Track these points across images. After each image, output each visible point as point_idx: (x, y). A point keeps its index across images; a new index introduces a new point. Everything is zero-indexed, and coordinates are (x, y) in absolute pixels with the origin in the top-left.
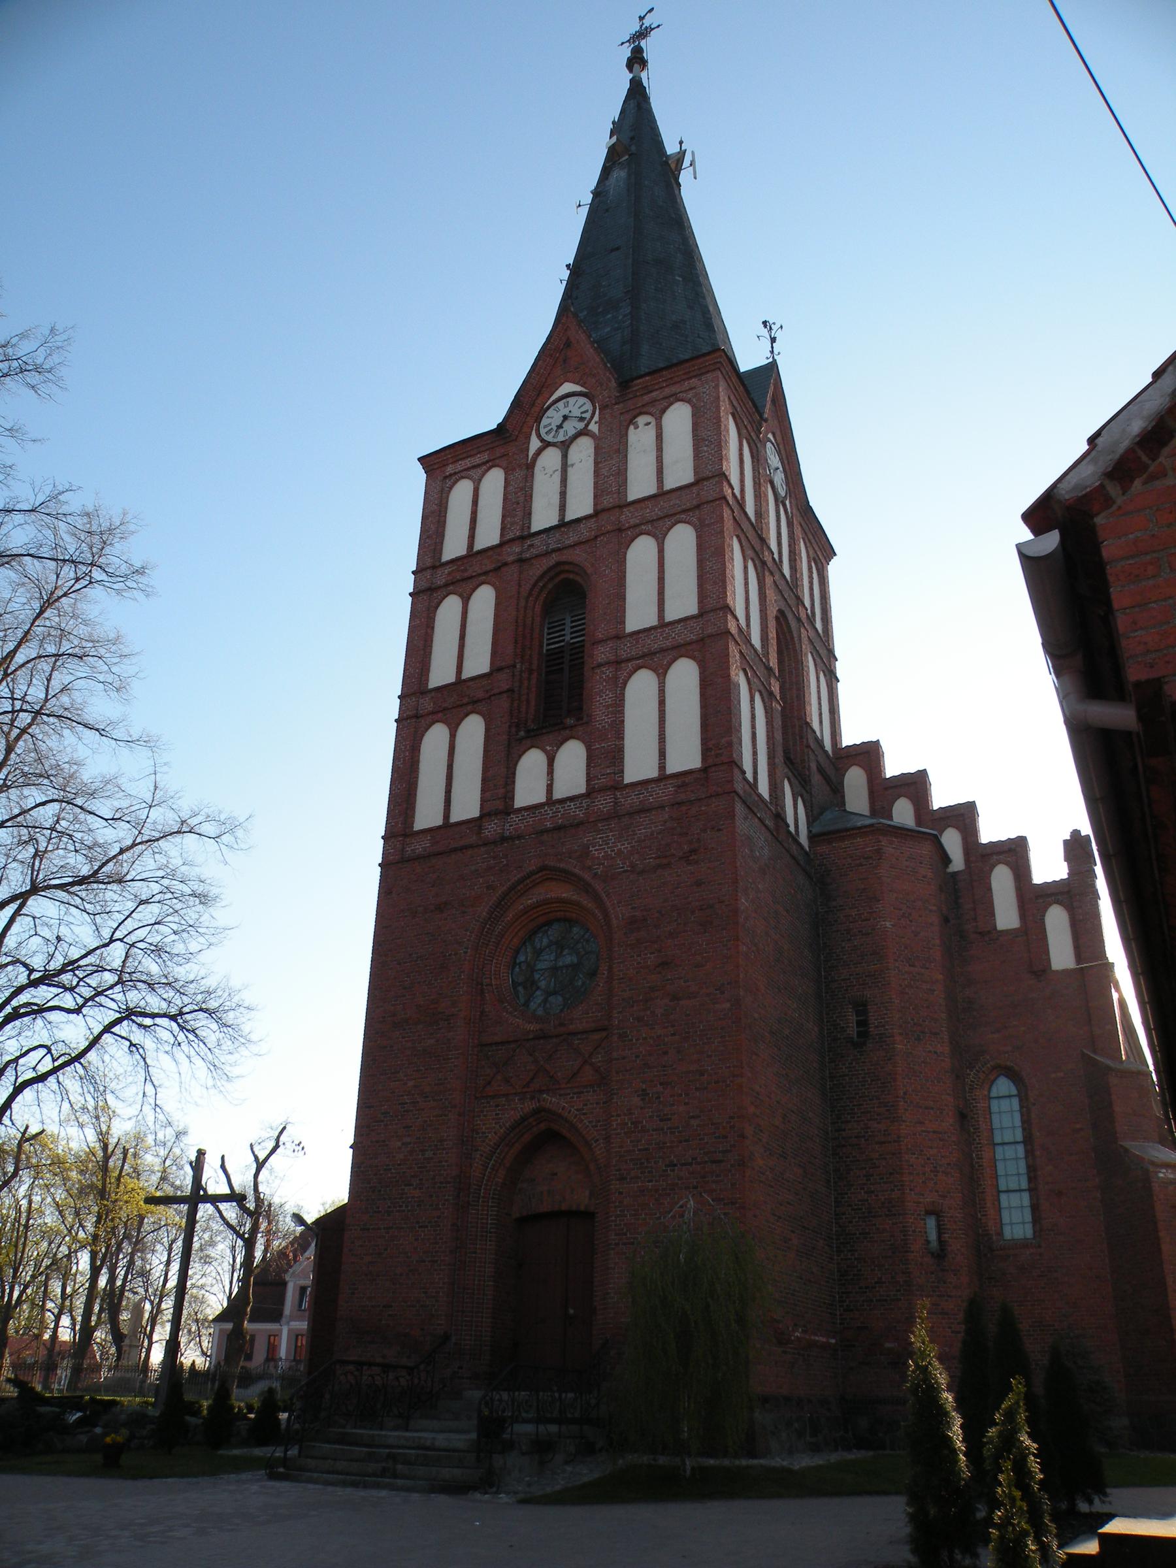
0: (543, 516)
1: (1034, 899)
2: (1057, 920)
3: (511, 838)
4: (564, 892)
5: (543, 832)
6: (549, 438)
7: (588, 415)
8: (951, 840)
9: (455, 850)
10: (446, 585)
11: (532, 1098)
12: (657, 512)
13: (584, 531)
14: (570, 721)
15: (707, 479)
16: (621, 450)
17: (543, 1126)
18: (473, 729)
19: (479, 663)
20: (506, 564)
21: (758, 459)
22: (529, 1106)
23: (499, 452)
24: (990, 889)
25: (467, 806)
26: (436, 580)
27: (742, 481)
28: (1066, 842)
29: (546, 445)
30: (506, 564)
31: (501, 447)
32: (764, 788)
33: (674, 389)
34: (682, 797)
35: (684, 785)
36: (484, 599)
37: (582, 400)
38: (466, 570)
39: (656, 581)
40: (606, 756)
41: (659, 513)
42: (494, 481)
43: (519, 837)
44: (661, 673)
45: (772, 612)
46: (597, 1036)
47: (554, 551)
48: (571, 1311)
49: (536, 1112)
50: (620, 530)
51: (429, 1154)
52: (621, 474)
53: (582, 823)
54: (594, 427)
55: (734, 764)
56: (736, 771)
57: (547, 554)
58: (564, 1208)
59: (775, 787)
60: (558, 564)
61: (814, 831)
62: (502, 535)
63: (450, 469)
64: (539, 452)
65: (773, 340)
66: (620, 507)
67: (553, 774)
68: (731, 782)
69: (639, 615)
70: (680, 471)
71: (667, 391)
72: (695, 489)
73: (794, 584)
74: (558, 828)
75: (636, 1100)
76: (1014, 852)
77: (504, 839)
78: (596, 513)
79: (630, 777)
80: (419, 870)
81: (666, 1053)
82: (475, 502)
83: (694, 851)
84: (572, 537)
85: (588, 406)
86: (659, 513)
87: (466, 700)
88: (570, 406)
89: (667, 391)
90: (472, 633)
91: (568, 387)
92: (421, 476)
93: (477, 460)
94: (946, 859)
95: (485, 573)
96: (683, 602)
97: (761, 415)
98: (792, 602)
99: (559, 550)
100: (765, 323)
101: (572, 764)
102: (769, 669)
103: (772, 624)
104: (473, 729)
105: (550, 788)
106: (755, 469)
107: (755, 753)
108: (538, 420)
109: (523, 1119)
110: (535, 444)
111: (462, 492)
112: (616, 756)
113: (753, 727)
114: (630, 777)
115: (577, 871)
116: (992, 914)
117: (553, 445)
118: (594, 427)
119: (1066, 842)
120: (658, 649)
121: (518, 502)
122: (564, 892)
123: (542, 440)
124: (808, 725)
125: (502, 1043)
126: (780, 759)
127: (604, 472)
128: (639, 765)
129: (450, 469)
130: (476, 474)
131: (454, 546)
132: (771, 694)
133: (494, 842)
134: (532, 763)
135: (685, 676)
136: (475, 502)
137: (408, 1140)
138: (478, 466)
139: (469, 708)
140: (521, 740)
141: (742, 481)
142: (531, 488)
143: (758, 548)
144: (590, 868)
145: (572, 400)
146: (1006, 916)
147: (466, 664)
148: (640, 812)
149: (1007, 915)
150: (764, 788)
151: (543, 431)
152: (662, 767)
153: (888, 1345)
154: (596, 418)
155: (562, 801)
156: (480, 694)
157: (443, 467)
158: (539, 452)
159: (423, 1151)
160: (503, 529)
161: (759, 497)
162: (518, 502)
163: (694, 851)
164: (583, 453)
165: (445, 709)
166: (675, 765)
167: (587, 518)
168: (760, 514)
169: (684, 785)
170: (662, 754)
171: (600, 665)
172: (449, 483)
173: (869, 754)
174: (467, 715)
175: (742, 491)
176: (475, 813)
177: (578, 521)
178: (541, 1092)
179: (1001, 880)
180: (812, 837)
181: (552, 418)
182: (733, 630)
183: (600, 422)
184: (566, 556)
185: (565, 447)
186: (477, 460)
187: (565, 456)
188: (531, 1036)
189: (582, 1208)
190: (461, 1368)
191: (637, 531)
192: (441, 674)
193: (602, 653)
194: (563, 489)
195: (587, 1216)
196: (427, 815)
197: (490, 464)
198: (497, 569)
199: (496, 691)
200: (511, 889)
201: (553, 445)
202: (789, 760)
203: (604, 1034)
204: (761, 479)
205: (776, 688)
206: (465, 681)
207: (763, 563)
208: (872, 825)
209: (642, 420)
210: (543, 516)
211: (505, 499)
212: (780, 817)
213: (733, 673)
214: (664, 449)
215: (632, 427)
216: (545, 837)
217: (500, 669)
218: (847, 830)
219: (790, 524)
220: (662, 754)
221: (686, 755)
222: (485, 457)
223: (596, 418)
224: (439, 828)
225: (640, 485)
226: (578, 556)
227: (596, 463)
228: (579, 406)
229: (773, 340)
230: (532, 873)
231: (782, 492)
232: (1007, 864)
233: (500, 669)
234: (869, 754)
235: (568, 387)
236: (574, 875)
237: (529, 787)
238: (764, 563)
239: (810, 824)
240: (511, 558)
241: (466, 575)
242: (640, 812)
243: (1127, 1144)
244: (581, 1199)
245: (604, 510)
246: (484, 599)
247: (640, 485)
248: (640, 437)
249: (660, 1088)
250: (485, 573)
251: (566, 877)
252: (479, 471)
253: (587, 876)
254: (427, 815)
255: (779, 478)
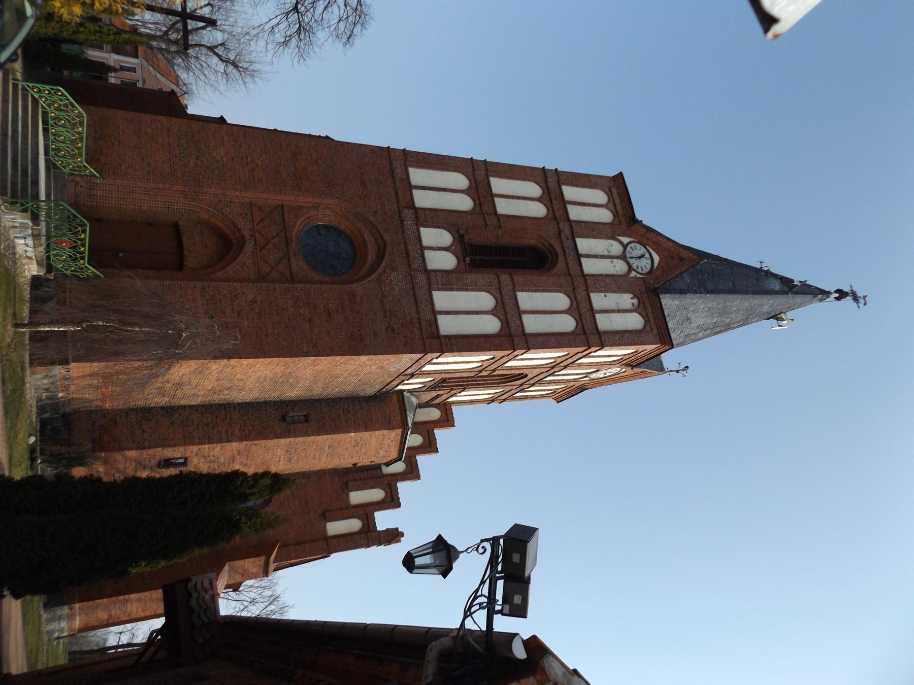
0: (584, 245)
1: (366, 512)
2: (354, 524)
3: (402, 226)
4: (371, 256)
5: (405, 244)
6: (628, 249)
7: (640, 270)
8: (399, 467)
9: (396, 193)
10: (548, 188)
11: (251, 236)
12: (583, 310)
13: (574, 270)
14: (468, 259)
15: (600, 339)
16: (619, 290)
17: (234, 241)
18: (464, 203)
19: (503, 207)
20: (558, 224)
21: (611, 364)
22: (247, 236)
23: (623, 219)
24: (371, 488)
25: (422, 199)
26: (551, 183)
27: (599, 356)
28: (397, 529)
29: (625, 247)
30: (558, 224)
31: (625, 220)
32: (428, 368)
33: (652, 319)
34: (423, 324)
35: (431, 325)
36: (538, 210)
37: (649, 267)
38: (556, 200)
39: (544, 309)
40: (448, 281)
41: (582, 311)
42: (605, 216)
43: (403, 230)
44: (493, 312)
45: (525, 372)
46: (288, 273)
47: (564, 252)
48: (121, 255)
49: (243, 238)
50: (574, 289)
51: (216, 172)
52: (606, 289)
53: (410, 266)
54: (633, 274)
55: (442, 351)
56: (438, 354)
57: (563, 247)
58: (186, 252)
59: (429, 373)
60: (557, 254)
61: (405, 393)
62: (575, 221)
63: (614, 191)
64: (621, 242)
65: (677, 371)
66: (587, 290)
67: (438, 249)
68: (432, 352)
69: (526, 299)
70: (604, 322)
71: (651, 316)
72: (595, 331)
73: (540, 382)
74: (408, 254)
75: (250, 297)
76: (392, 501)
77: (402, 221)
78: (584, 276)
79: (435, 294)
80: (385, 170)
81: (278, 314)
82: (595, 205)
83: (393, 331)
84: (572, 261)
85: (645, 271)
86: (582, 311)
87: (482, 200)
88: (645, 261)
89: (651, 316)
90: (519, 201)
91: (657, 259)
92: (612, 173)
93: (619, 207)
94: (388, 464)
95: (554, 212)
96: (532, 324)
97: (636, 366)
98: (532, 382)
99: (565, 254)
100: (687, 367)
101: (443, 261)
102: (494, 370)
103: (517, 372)
104: (464, 203)
105: (431, 248)
106: (605, 363)
107: (448, 363)
108: (639, 242)
109: (239, 230)
110: (625, 240)
111: (600, 197)
112: (448, 286)
113: (462, 362)
114: (435, 294)
115: (383, 264)
116: (357, 490)
117: (624, 251)
118: (633, 274)
119: (397, 529)
120: (506, 310)
121: (593, 230)
122: (371, 256)
123: (627, 244)
124: (464, 390)
125: (284, 219)
126: (445, 376)
127: (608, 280)
128: (442, 299)
129: (614, 191)
130: (611, 205)
131: (570, 192)
132: (481, 371)
133: (400, 216)
134: (444, 237)
135: (491, 325)
136: (595, 205)
137: (225, 159)
138: (615, 208)
139: (478, 202)
140: (458, 231)
141: (599, 356)
142: (601, 238)
143: (562, 365)
144: (384, 271)
145: (649, 261)
146: (357, 497)
147: (503, 200)
148: (416, 300)
149: (357, 497)
150: (428, 368)
151: (632, 245)
152: (441, 313)
153: (105, 437)
154: (638, 275)
155: (423, 256)
156: (485, 208)
157: (617, 188)
158: (621, 242)
159: (218, 168)
160: (579, 222)
161: (590, 365)
162: (593, 230)
163: (393, 331)
164: (619, 267)
165: (477, 187)
166: (441, 319)
167: (582, 270)
168: (580, 365)
169: (431, 325)
170: (448, 313)
171: (498, 278)
172: (607, 190)
173: (447, 420)
174: (474, 200)
175: (593, 357)
176: (418, 204)
177: (580, 265)
178: (255, 241)
179: (377, 494)
180: (402, 391)
181: (639, 250)
182: (516, 353)
183: (635, 277)
184: (561, 258)
185: (623, 257)
186: (619, 207)
187: (617, 257)
188: (288, 235)
189: (185, 263)
190: (82, 187)
191: (573, 298)
192: (498, 185)
193: (505, 278)
194: (599, 256)
195: (180, 267)
196: (417, 176)
197: (615, 214)
198: (555, 218)
199: (487, 218)
200: (374, 226)
201: (624, 251)
202: (444, 380)
203: (289, 278)
204: (599, 366)
205: (484, 373)
206: (493, 199)
207: (552, 368)
208: (407, 425)
209: (635, 301)
210: (584, 245)
211: (595, 223)
212: (412, 376)
213: (492, 352)
214: (617, 311)
215: (631, 296)
216: (403, 245)
217: (499, 220)
218: (405, 411)
219: (575, 380)
220: (448, 313)
221: (447, 325)
222: (620, 211)
223: (638, 275)
224: (409, 183)
225: (599, 300)
226: (560, 266)
227: (612, 276)
228: (644, 265)
229: (677, 371)
230: (382, 237)
231: (593, 376)
232: (385, 497)
233: (499, 220)
234: (447, 420)
235: (657, 259)
236: (381, 262)
237: (432, 236)
238: (553, 367)
239: (409, 391)
240: (561, 226)
241: (553, 200)
242: (416, 300)
243: (226, 568)
244: (191, 262)
245: (586, 280)
246: (538, 210)
247: (599, 300)
248: (626, 300)
249: (257, 311)
250: (554, 212)
251: (380, 257)
252: (612, 208)
253: (380, 270)
254: (417, 176)
255: (600, 375)
